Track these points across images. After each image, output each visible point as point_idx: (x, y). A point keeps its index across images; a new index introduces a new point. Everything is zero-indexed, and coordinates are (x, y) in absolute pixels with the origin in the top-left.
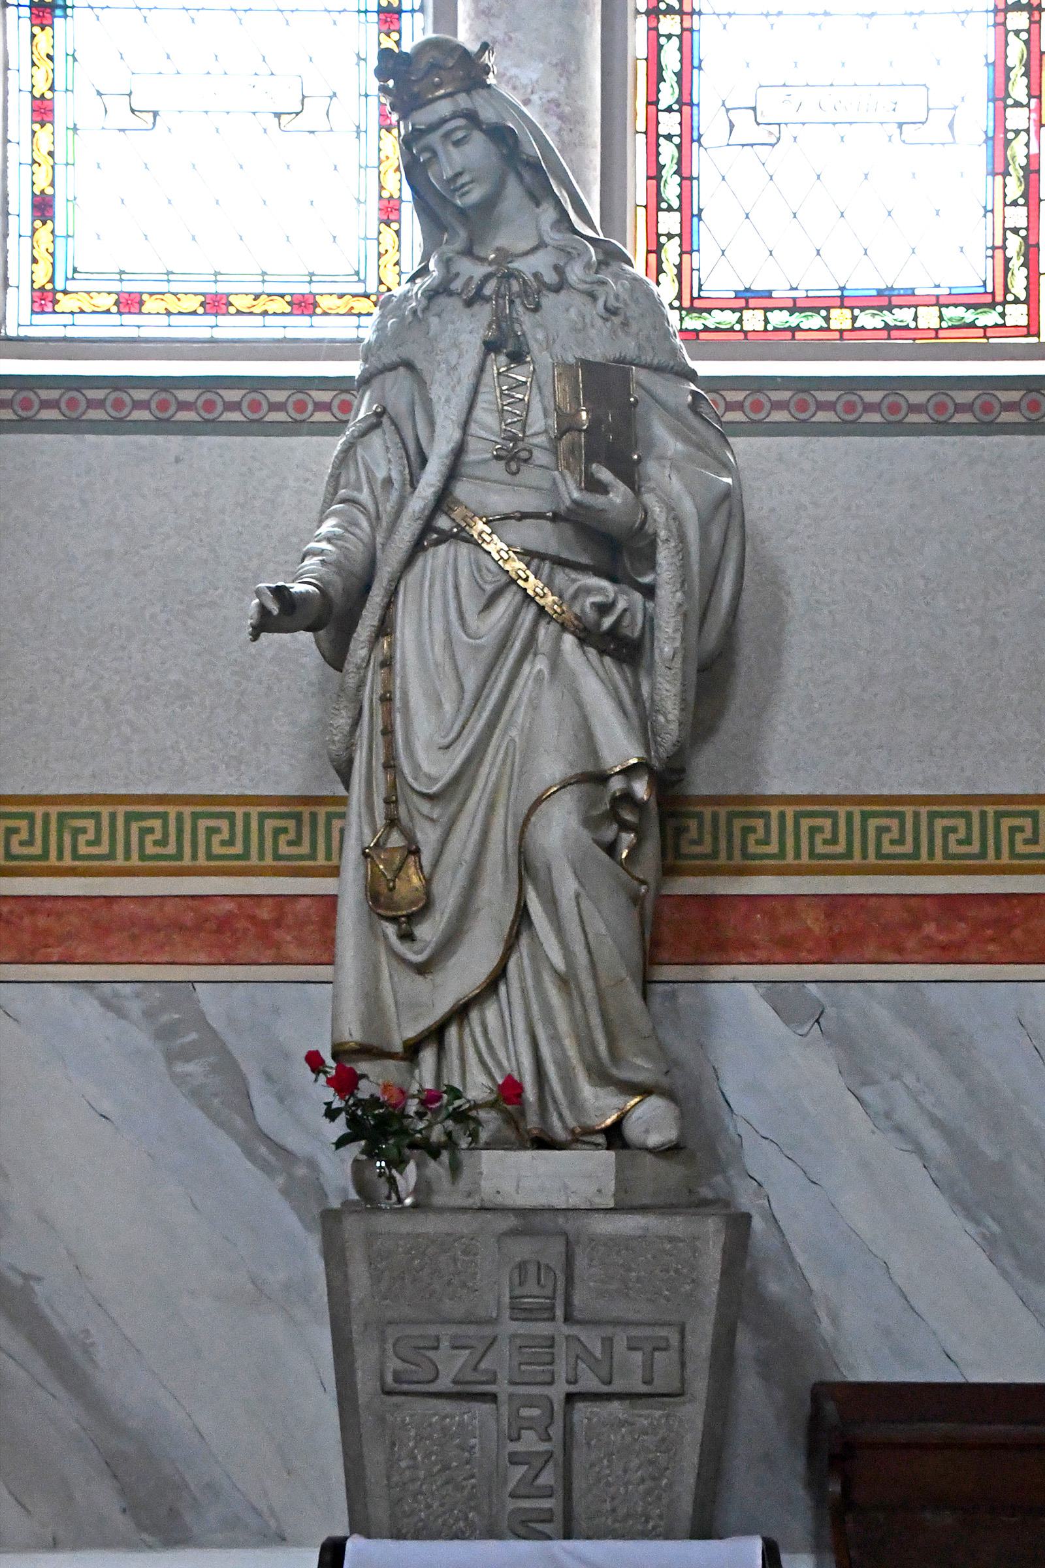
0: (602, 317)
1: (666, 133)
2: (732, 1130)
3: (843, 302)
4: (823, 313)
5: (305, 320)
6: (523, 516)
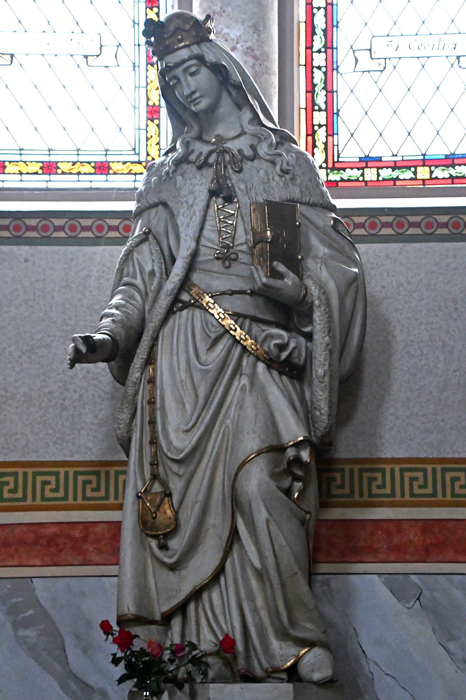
0: (279, 175)
1: (317, 65)
2: (367, 670)
3: (424, 162)
4: (413, 169)
5: (103, 177)
6: (233, 293)
